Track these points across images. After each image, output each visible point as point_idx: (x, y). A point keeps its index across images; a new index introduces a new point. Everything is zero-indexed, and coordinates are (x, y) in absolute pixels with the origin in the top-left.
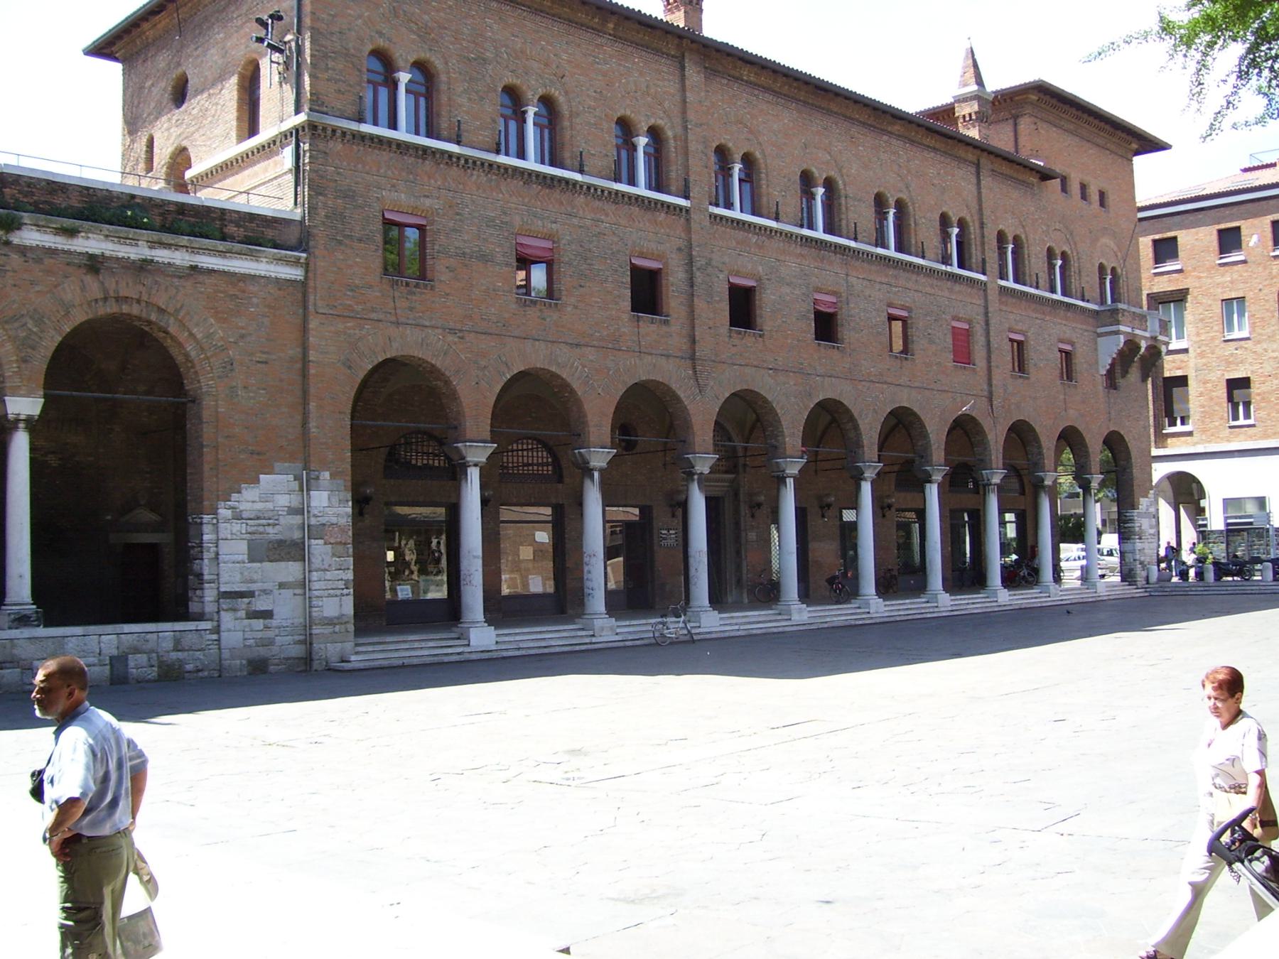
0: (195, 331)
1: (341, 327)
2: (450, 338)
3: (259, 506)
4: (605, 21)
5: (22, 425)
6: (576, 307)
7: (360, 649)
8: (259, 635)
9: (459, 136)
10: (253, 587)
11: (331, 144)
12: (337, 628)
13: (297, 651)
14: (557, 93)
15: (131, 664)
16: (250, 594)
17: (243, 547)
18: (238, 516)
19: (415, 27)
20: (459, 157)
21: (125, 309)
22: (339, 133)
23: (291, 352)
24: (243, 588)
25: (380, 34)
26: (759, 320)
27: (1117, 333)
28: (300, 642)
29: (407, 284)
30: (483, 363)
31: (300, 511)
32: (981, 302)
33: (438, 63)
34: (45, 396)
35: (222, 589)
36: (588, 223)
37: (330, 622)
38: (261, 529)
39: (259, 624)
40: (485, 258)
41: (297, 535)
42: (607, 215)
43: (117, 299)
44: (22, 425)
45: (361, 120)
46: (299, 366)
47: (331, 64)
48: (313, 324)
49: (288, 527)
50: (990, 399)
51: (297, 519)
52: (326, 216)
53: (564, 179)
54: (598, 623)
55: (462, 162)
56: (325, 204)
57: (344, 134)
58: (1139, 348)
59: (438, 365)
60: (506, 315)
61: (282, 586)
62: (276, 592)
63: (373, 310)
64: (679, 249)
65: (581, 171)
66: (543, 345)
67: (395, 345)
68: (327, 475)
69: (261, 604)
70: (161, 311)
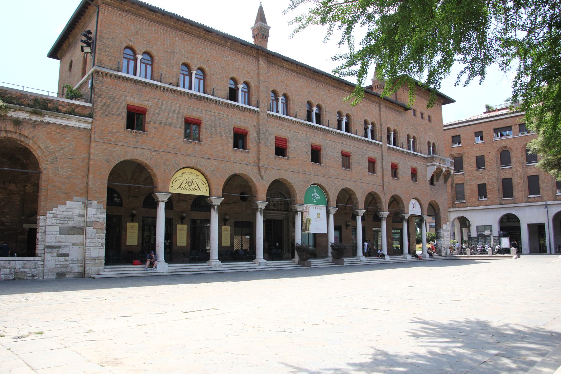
0: (40, 145)
1: (105, 146)
2: (154, 153)
3: (66, 213)
6: (209, 145)
7: (106, 270)
8: (62, 263)
9: (213, 93)
10: (61, 244)
11: (105, 79)
12: (97, 262)
13: (78, 270)
16: (60, 247)
17: (57, 229)
18: (55, 217)
19: (145, 39)
23: (84, 156)
24: (57, 244)
25: (130, 40)
26: (287, 153)
27: (434, 165)
31: (83, 216)
32: (380, 152)
33: (154, 53)
35: (47, 244)
36: (216, 114)
37: (94, 259)
38: (66, 222)
39: (62, 258)
40: (170, 125)
42: (224, 112)
43: (6, 131)
45: (178, 85)
46: (87, 161)
47: (107, 50)
48: (93, 145)
49: (78, 222)
50: (383, 186)
52: (102, 106)
55: (162, 89)
56: (101, 101)
57: (111, 75)
58: (442, 171)
59: (148, 163)
60: (179, 146)
61: (74, 244)
62: (71, 247)
63: (120, 141)
64: (255, 126)
65: (213, 95)
68: (96, 202)
69: (63, 251)
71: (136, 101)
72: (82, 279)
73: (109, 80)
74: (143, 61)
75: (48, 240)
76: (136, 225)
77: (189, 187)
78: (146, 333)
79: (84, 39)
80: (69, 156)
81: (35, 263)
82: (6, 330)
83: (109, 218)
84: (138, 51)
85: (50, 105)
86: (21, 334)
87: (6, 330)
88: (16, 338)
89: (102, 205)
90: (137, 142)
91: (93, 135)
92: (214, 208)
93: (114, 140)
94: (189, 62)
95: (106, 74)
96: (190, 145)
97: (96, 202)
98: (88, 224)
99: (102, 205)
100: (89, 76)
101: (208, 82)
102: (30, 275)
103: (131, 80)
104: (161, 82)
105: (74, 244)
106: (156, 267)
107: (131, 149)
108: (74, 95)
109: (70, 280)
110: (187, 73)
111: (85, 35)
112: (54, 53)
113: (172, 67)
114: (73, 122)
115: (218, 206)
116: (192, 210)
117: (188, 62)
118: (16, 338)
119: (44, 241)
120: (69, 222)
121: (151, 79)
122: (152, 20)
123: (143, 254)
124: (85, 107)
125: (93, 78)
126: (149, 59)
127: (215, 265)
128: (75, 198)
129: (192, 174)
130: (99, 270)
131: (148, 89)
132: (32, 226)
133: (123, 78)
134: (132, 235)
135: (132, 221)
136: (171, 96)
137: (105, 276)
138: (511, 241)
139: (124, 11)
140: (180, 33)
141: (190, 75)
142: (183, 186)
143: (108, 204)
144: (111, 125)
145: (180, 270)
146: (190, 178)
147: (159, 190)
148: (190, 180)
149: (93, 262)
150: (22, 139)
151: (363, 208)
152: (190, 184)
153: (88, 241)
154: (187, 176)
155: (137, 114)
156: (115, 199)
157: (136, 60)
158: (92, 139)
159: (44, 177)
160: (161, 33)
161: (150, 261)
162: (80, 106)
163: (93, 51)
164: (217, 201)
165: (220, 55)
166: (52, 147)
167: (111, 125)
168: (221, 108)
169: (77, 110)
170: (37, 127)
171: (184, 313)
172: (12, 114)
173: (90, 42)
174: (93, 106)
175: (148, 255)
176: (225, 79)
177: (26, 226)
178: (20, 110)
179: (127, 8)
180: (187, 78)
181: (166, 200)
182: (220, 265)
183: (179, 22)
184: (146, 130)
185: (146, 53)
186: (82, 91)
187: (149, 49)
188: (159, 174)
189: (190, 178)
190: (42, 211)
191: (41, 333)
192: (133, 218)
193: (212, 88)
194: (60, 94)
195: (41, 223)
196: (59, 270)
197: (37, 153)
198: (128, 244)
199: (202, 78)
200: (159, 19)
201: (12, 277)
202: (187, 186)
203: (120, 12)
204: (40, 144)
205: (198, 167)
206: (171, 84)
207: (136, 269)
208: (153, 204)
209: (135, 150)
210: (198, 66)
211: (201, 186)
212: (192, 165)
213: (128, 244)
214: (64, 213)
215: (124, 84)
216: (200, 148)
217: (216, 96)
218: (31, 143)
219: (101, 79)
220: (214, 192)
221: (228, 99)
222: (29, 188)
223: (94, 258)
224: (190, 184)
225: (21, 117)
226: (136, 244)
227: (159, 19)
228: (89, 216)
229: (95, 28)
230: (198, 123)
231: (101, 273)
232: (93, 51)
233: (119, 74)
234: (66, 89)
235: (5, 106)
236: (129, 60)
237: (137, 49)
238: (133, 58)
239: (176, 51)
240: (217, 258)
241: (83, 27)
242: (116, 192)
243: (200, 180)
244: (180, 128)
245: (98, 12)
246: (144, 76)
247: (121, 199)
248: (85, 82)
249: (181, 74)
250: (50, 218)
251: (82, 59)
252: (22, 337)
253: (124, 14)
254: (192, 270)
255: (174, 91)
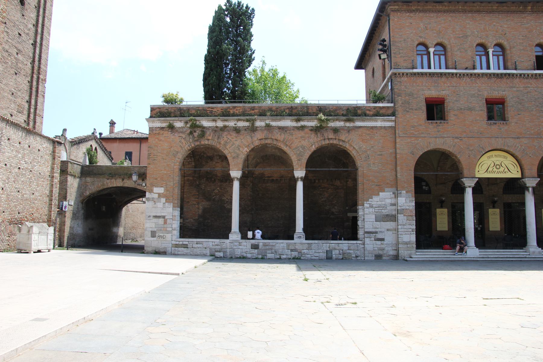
0: (355, 147)
1: (409, 140)
2: (456, 140)
3: (380, 203)
4: (525, 7)
5: (300, 179)
6: (516, 123)
7: (417, 253)
8: (379, 246)
9: (516, 66)
10: (377, 230)
11: (402, 79)
12: (409, 246)
13: (392, 253)
14: (503, 41)
15: (333, 253)
16: (376, 233)
17: (374, 217)
18: (371, 206)
19: (435, 32)
20: (456, 74)
21: (331, 142)
22: (405, 74)
23: (391, 151)
24: (374, 230)
25: (421, 37)
28: (395, 250)
29: (436, 123)
30: (471, 149)
31: (394, 205)
33: (446, 42)
34: (306, 170)
35: (366, 230)
36: (522, 89)
37: (406, 243)
38: (380, 211)
39: (379, 243)
40: (470, 109)
41: (394, 213)
42: (531, 84)
43: (328, 139)
44: (300, 179)
45: (474, 68)
46: (394, 155)
47: (401, 52)
48: (398, 140)
49: (390, 210)
51: (394, 207)
52: (402, 103)
53: (507, 73)
54: (531, 250)
55: (458, 75)
56: (401, 99)
57: (407, 74)
59: (451, 150)
60: (482, 130)
61: (388, 230)
62: (386, 232)
63: (422, 133)
65: (516, 69)
66: (500, 139)
67: (432, 145)
68: (404, 192)
69: (379, 236)
70: (344, 141)
71: (433, 93)
72: (395, 260)
73: (406, 79)
74: (435, 53)
75: (366, 226)
76: (445, 211)
77: (497, 170)
78: (441, 314)
79: (381, 47)
80: (379, 153)
81: (358, 246)
82: (331, 298)
83: (418, 205)
84: (430, 45)
85: (359, 112)
86: (342, 302)
87: (331, 298)
88: (337, 305)
89: (410, 194)
90: (438, 131)
91: (397, 132)
92: (528, 190)
93: (416, 133)
94: (484, 41)
95: (403, 74)
96: (493, 127)
97: (404, 192)
98: (399, 211)
99: (410, 194)
100: (388, 79)
101: (509, 56)
102: (354, 256)
103: (426, 74)
104: (456, 69)
105: (388, 230)
106: (466, 252)
107: (433, 139)
108: (378, 99)
109: (386, 261)
110: (483, 53)
111: (381, 44)
112: (359, 66)
113: (466, 51)
114: (379, 123)
115: (534, 188)
116: (504, 193)
117: (483, 41)
118: (337, 305)
119: (364, 227)
120: (383, 211)
121: (446, 69)
122: (440, 11)
123: (453, 239)
124: (388, 107)
125: (392, 80)
126: (442, 49)
127: (534, 252)
128: (386, 189)
129: (500, 156)
130: (411, 254)
131: (444, 79)
132: (354, 214)
133: (418, 73)
134: (442, 221)
135: (442, 207)
136: (468, 80)
137: (417, 259)
138: (166, 200)
139: (411, 11)
140: (470, 15)
141: (487, 55)
142: (490, 169)
143: (416, 192)
144: (412, 119)
145: (492, 256)
146: (498, 160)
147: (465, 176)
148: (498, 163)
149: (406, 246)
150: (341, 144)
151: (536, 175)
152: (498, 167)
153: (400, 227)
154: (494, 159)
155: (437, 105)
156: (424, 187)
157: (428, 54)
158: (397, 135)
159: (360, 173)
160: (450, 21)
161: (460, 247)
162: (384, 107)
163: (389, 57)
164: (531, 182)
165: (519, 24)
166: (363, 146)
167: (412, 119)
168: (528, 80)
169: (381, 112)
170: (350, 132)
171: (484, 299)
172: (332, 124)
173: (386, 49)
174: (395, 105)
175: (458, 240)
176: (529, 48)
177: (350, 215)
178: (337, 120)
179: (413, 8)
180: (484, 59)
181: (473, 185)
182: (539, 253)
183: (467, 4)
184: (446, 119)
185: (438, 44)
186: (384, 94)
187: (439, 40)
188: (463, 160)
189: (498, 160)
190: (360, 202)
191: (355, 303)
192: (442, 204)
193: (513, 61)
194: (368, 101)
195: (360, 213)
196: (377, 252)
197: (353, 153)
198: (438, 229)
199: (501, 53)
200: (447, 8)
201: (341, 257)
202: (495, 169)
203: (408, 14)
204: (355, 145)
205: (506, 148)
206: (466, 69)
207: (445, 253)
208: (460, 190)
209: (437, 140)
210: (495, 42)
211: (511, 167)
212: (498, 147)
213: (438, 229)
214: (378, 203)
215: (420, 79)
216: (506, 127)
217: (519, 69)
218: (347, 146)
219: (399, 79)
220: (527, 172)
221: (534, 70)
222: (350, 183)
223: (406, 242)
224: (498, 167)
225: (338, 125)
226: (446, 229)
227: (447, 8)
228: (399, 205)
229: (388, 35)
230: (501, 102)
231: (413, 256)
232: (389, 57)
233: (415, 71)
234: (374, 96)
235: (326, 119)
236: (422, 55)
237: (428, 43)
238: (425, 52)
239: (468, 34)
240: (535, 244)
241: (379, 37)
242: (425, 181)
243: (509, 161)
244: (481, 110)
245: (389, 20)
246: (438, 67)
247: (429, 188)
248: (386, 85)
249: (477, 55)
250: (367, 208)
251: (381, 65)
252: (342, 305)
253: (412, 15)
254: (505, 256)
255: (471, 74)
